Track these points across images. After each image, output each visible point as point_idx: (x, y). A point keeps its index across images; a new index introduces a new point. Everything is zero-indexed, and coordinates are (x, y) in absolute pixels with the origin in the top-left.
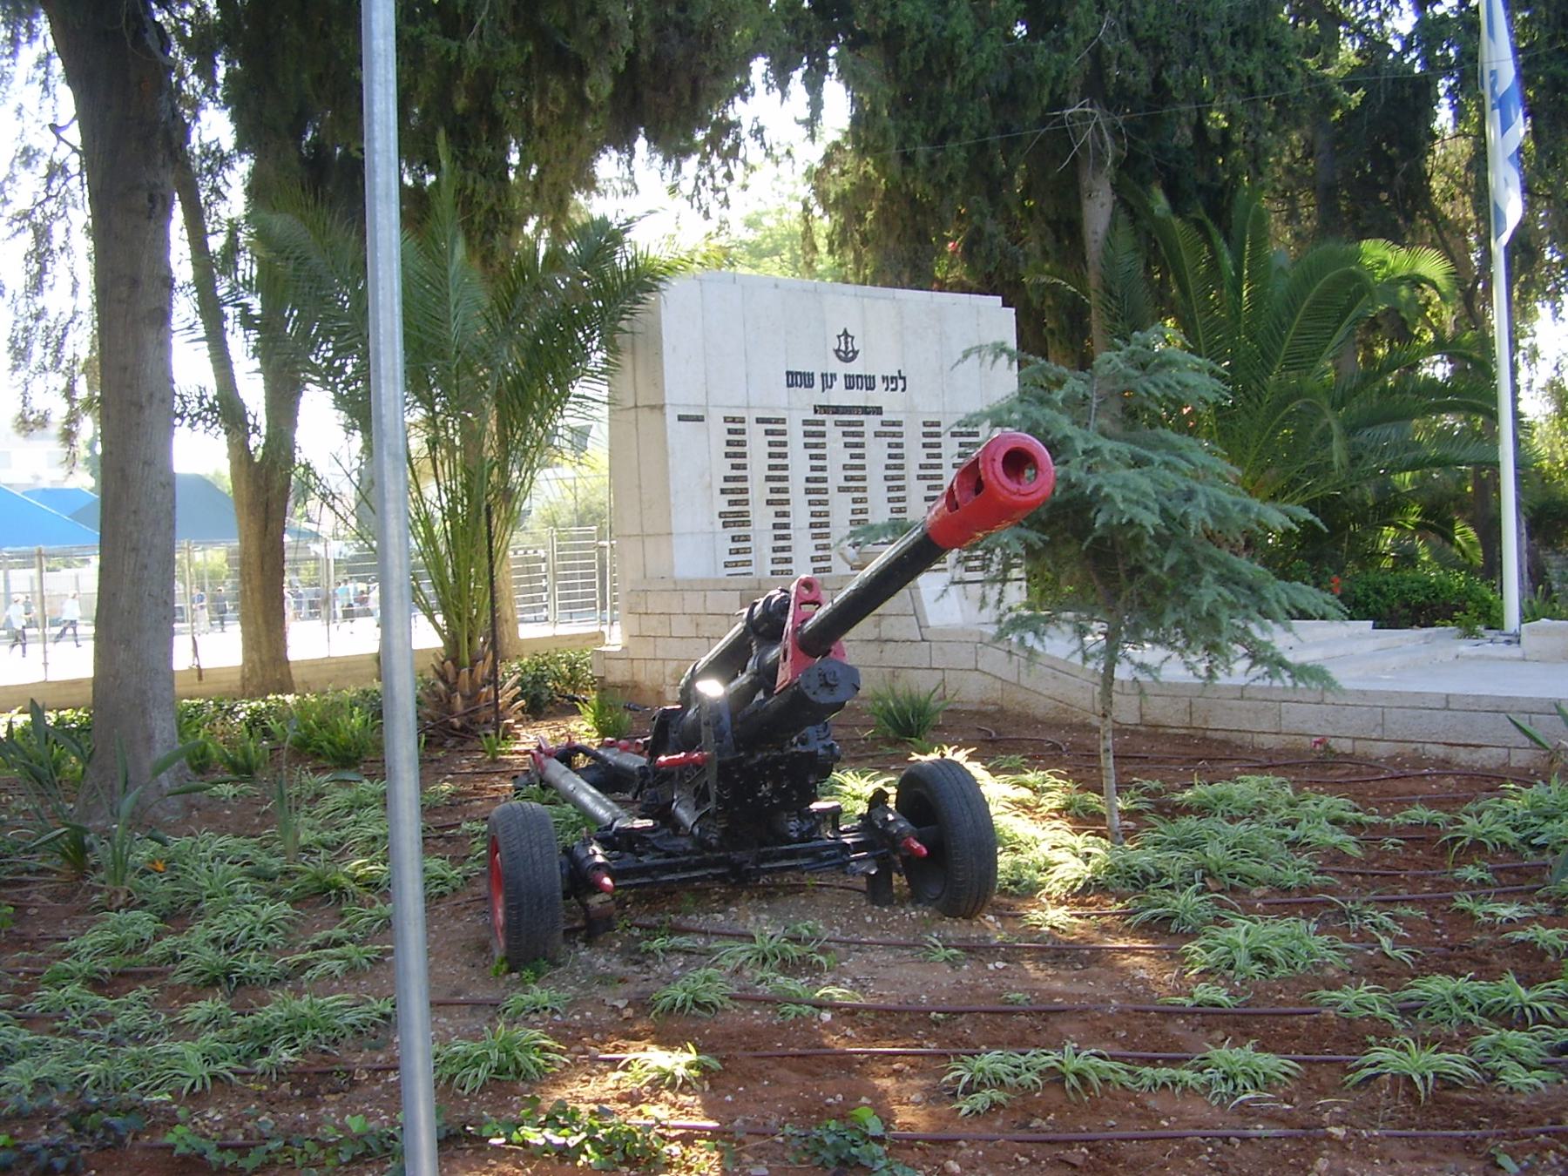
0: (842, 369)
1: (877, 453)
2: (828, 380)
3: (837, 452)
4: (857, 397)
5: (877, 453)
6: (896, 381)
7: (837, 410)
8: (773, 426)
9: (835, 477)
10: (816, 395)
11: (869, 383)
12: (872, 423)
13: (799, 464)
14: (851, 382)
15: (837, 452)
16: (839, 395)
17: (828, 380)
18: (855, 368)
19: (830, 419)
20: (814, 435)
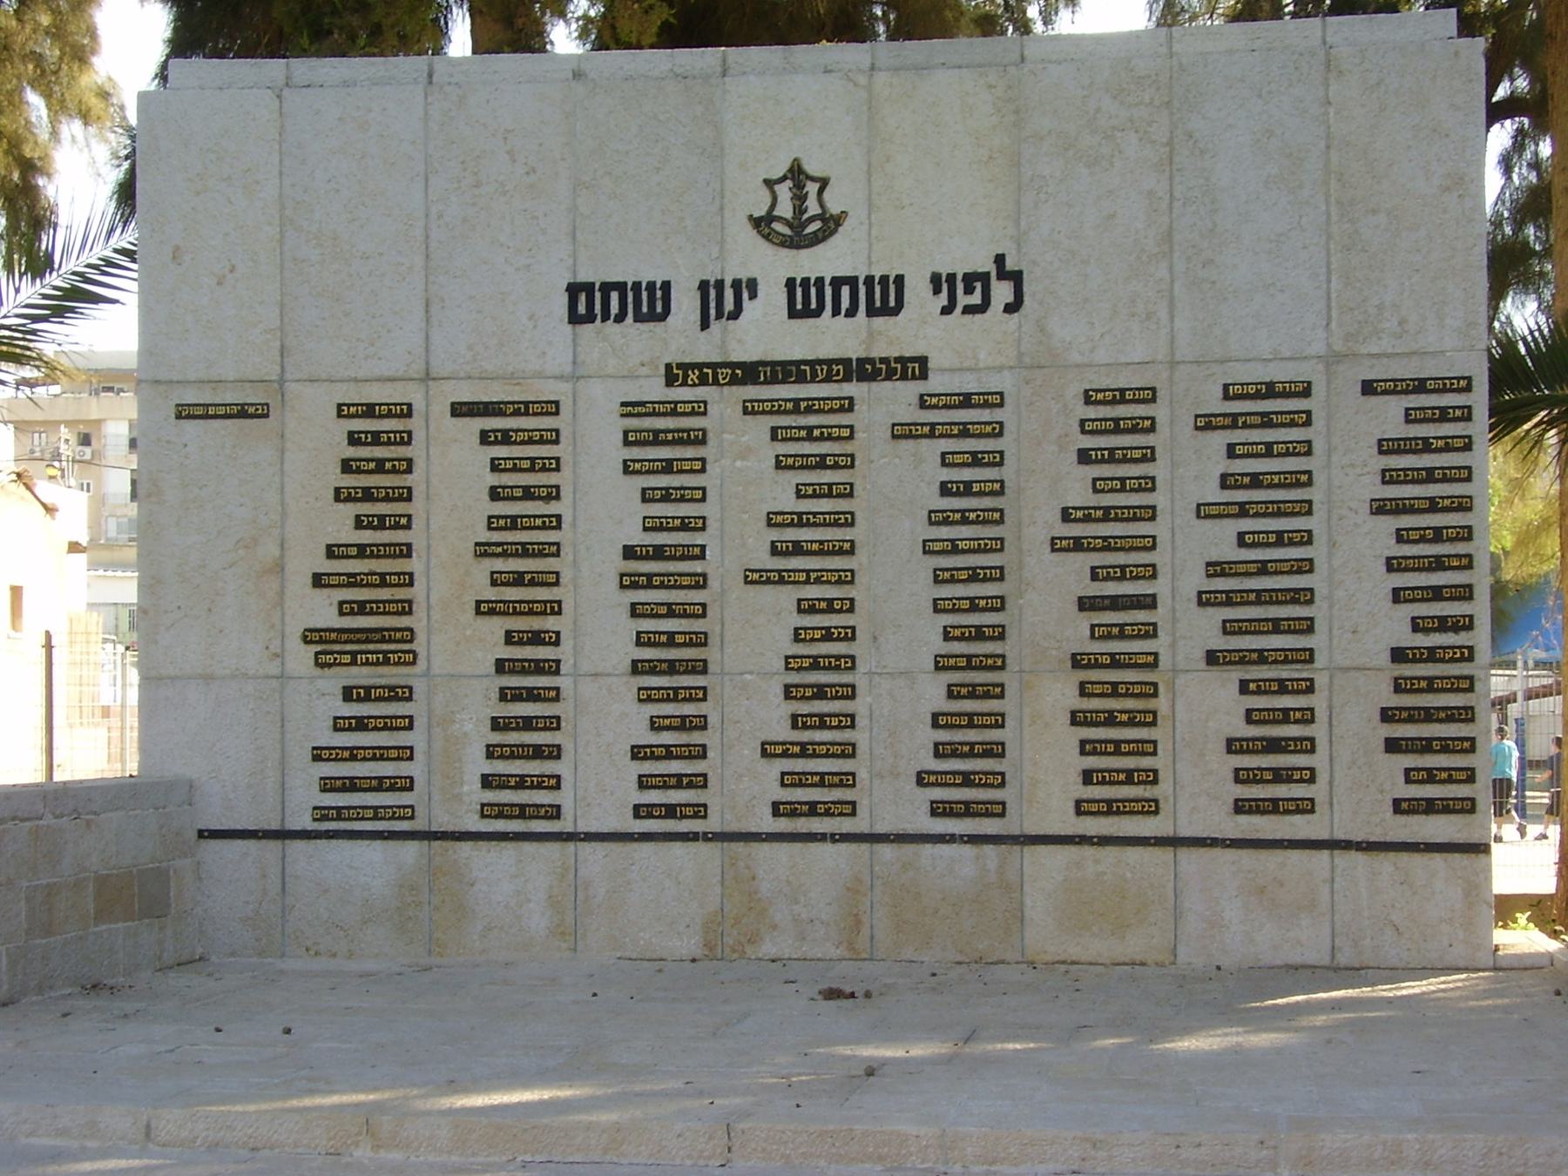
0: (774, 267)
1: (896, 488)
2: (721, 300)
4: (835, 336)
5: (896, 488)
7: (749, 373)
8: (517, 431)
9: (735, 535)
10: (682, 336)
11: (884, 296)
13: (602, 510)
14: (804, 300)
16: (766, 331)
17: (721, 300)
19: (724, 402)
20: (663, 443)
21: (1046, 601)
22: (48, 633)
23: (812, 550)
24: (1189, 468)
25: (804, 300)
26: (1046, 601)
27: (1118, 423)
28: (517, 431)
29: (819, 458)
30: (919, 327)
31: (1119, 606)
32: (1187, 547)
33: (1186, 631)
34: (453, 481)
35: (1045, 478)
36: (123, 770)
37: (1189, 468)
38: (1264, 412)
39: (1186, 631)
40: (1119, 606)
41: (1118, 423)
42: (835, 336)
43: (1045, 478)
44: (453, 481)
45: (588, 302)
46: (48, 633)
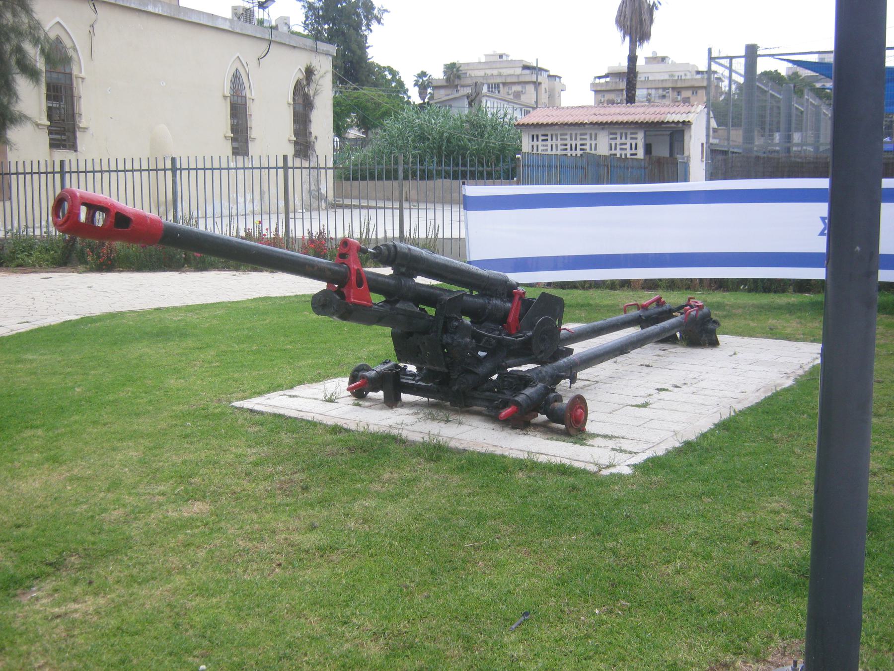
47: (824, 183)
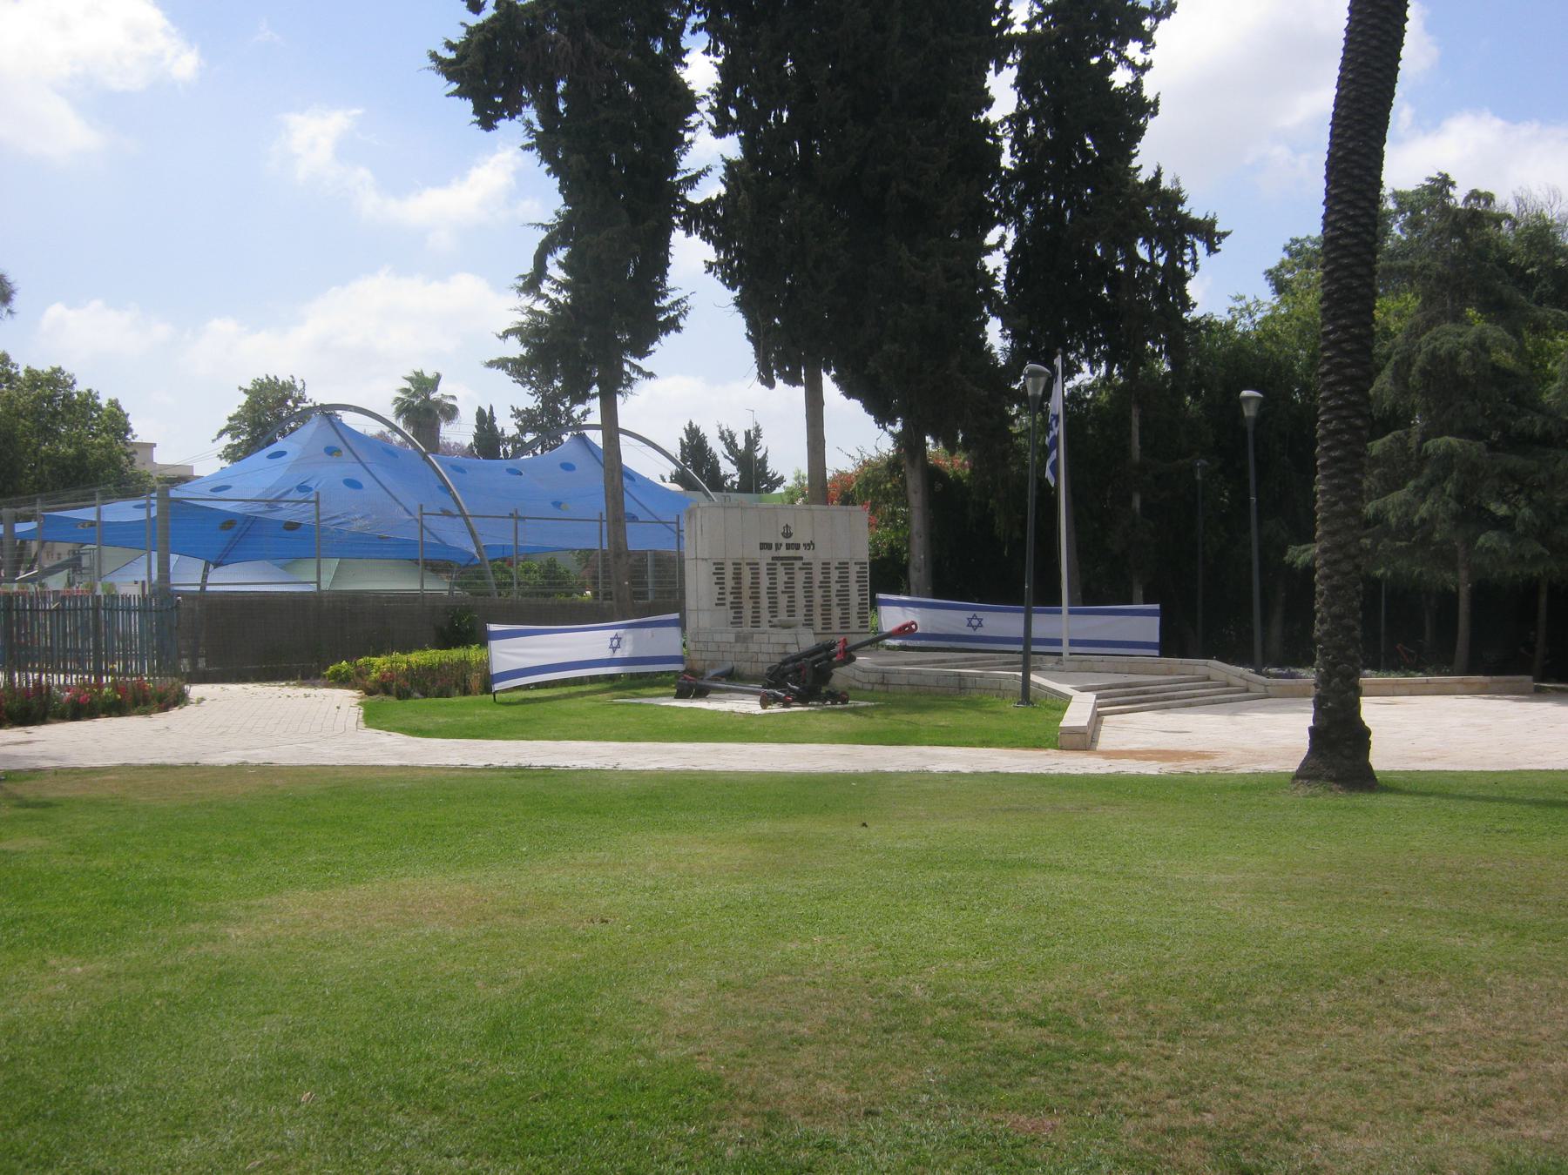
0: (784, 541)
1: (800, 577)
2: (778, 546)
3: (782, 577)
4: (792, 553)
5: (800, 577)
6: (810, 546)
8: (754, 567)
9: (781, 587)
11: (797, 547)
12: (798, 564)
13: (765, 582)
14: (789, 547)
15: (782, 577)
16: (783, 552)
17: (778, 546)
18: (790, 541)
21: (818, 594)
22: (491, 364)
23: (790, 587)
24: (835, 575)
25: (789, 547)
26: (818, 594)
27: (826, 566)
28: (754, 567)
29: (790, 573)
30: (802, 552)
31: (826, 598)
32: (835, 587)
33: (835, 600)
34: (747, 575)
35: (818, 577)
36: (204, 584)
37: (835, 575)
38: (843, 567)
39: (835, 600)
40: (826, 598)
41: (826, 566)
42: (792, 553)
43: (818, 577)
44: (747, 575)
45: (765, 546)
46: (491, 364)
47: (1157, 607)
